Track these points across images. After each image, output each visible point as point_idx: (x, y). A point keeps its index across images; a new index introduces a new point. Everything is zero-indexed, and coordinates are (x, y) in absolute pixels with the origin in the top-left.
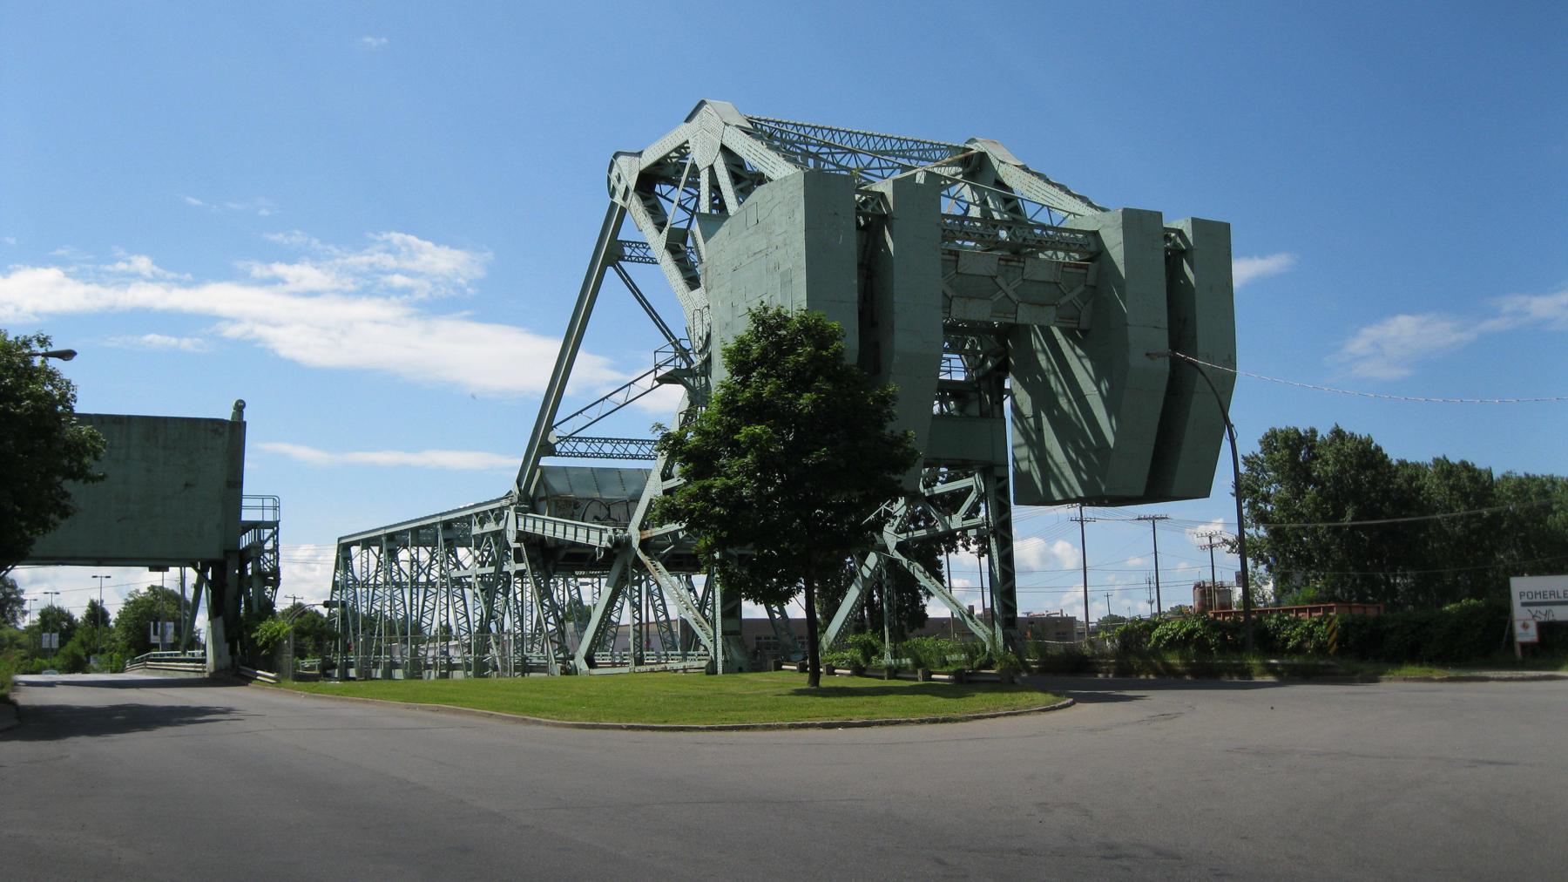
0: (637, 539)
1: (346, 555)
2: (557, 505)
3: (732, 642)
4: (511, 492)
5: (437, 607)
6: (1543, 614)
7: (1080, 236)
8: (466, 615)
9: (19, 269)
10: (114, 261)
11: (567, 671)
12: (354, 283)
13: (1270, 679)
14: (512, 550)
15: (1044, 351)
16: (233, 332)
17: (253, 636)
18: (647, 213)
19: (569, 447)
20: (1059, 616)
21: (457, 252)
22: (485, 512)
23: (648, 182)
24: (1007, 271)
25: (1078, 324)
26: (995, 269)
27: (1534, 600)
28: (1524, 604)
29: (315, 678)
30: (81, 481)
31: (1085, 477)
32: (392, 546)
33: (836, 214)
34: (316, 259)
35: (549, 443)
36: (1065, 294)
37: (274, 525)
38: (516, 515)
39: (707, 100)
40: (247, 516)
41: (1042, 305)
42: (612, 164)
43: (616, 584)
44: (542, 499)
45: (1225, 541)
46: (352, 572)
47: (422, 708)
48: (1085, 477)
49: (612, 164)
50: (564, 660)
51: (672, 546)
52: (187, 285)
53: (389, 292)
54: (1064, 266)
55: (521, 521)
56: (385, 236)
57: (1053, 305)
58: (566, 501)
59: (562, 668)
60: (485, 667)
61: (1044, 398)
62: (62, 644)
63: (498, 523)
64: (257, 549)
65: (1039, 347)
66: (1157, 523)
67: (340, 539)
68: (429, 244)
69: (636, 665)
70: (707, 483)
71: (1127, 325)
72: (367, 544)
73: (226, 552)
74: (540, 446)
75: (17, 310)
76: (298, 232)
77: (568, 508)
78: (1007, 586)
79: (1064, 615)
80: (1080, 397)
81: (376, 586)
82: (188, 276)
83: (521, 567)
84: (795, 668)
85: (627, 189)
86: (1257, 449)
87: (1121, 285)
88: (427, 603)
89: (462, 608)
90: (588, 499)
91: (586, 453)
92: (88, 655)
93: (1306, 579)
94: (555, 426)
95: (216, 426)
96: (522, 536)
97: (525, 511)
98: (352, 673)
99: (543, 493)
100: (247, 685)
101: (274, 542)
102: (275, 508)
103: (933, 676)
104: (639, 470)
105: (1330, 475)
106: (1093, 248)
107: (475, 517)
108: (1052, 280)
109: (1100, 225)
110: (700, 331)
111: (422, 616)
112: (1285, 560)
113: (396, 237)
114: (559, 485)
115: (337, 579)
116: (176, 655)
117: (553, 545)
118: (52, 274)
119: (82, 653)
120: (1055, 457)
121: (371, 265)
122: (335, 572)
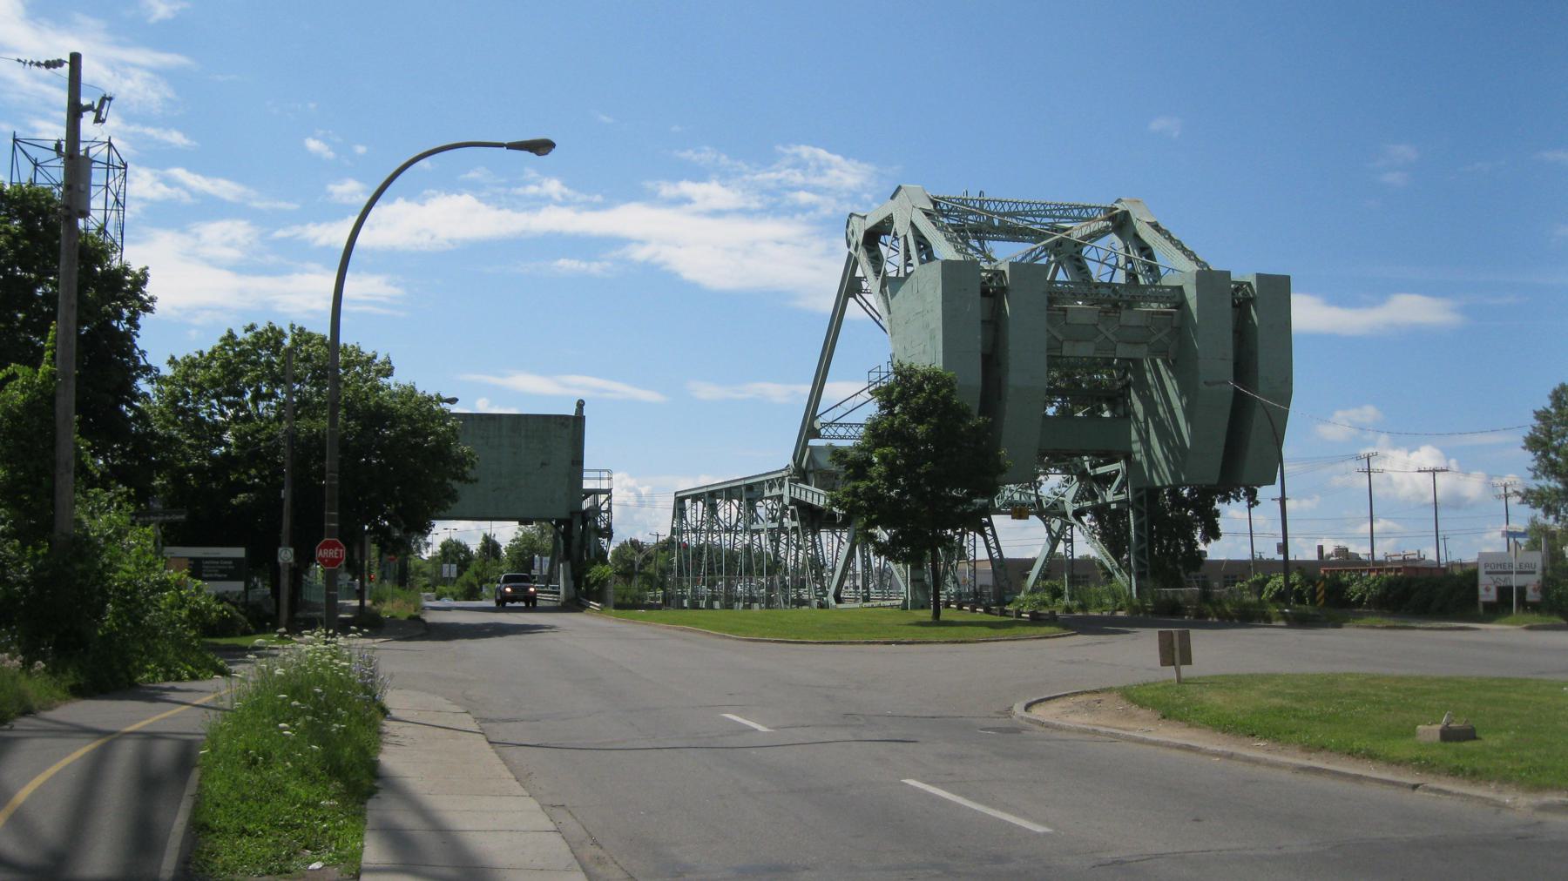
1: (681, 506)
2: (821, 477)
4: (788, 465)
6: (1502, 581)
7: (1168, 290)
9: (434, 196)
10: (524, 184)
11: (822, 606)
12: (759, 201)
13: (1282, 623)
15: (1150, 371)
16: (640, 254)
17: (587, 576)
20: (1416, 557)
21: (866, 166)
22: (772, 480)
27: (1496, 570)
28: (1487, 573)
29: (659, 607)
30: (463, 482)
34: (725, 177)
37: (608, 491)
39: (903, 186)
40: (587, 485)
41: (1136, 343)
44: (811, 472)
45: (1517, 493)
46: (686, 520)
47: (677, 629)
48: (1173, 468)
50: (820, 597)
52: (596, 207)
53: (795, 210)
56: (795, 150)
61: (1150, 408)
62: (460, 573)
66: (1438, 475)
68: (837, 158)
70: (857, 484)
73: (572, 513)
74: (808, 431)
75: (433, 237)
76: (707, 148)
82: (598, 198)
83: (795, 524)
86: (1547, 403)
89: (758, 541)
92: (481, 584)
94: (820, 415)
97: (797, 482)
99: (811, 468)
100: (582, 612)
103: (1023, 615)
106: (1177, 299)
113: (805, 151)
115: (675, 526)
116: (542, 587)
118: (466, 200)
119: (475, 581)
121: (779, 181)
122: (673, 520)
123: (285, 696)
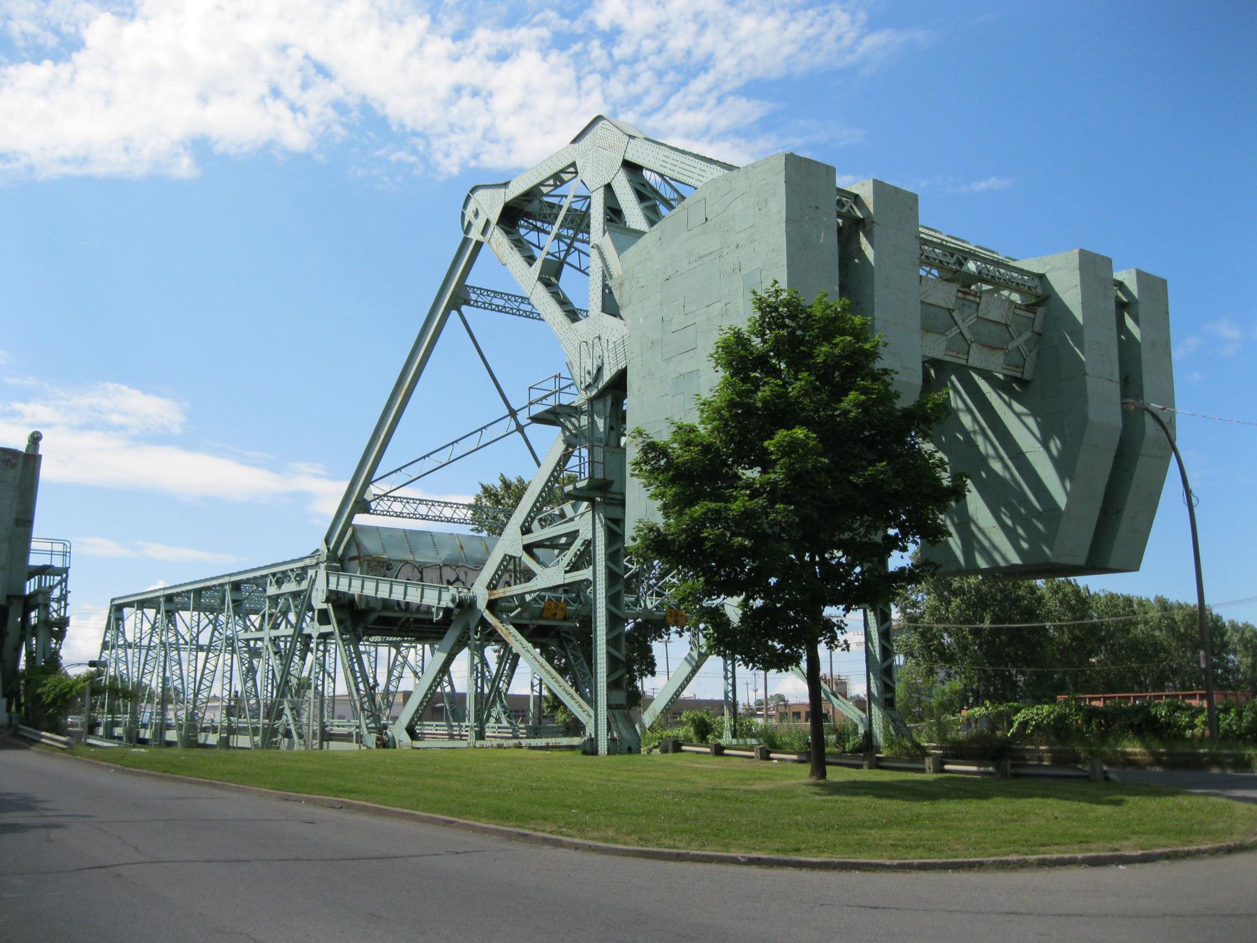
0: (484, 599)
1: (118, 615)
2: (369, 566)
3: (617, 716)
4: (318, 550)
5: (156, 671)
8: (182, 678)
14: (316, 612)
15: (969, 410)
18: (513, 247)
19: (384, 505)
23: (512, 216)
24: (964, 305)
25: (1023, 373)
26: (954, 301)
31: (1025, 545)
32: (171, 607)
33: (817, 208)
35: (365, 501)
36: (1013, 339)
38: (327, 573)
40: (35, 560)
41: (993, 348)
42: (468, 198)
43: (452, 649)
46: (123, 633)
48: (1025, 545)
49: (468, 198)
51: (519, 609)
54: (1015, 307)
55: (333, 579)
57: (1002, 349)
58: (379, 562)
59: (378, 739)
60: (275, 732)
63: (299, 583)
64: (40, 600)
65: (961, 405)
67: (113, 600)
69: (476, 739)
71: (1085, 374)
72: (142, 604)
73: (9, 597)
74: (356, 502)
77: (381, 567)
78: (887, 663)
79: (697, 698)
80: (1018, 456)
81: (149, 648)
83: (326, 629)
84: (708, 750)
85: (488, 223)
87: (1077, 331)
88: (147, 666)
89: (178, 672)
90: (401, 561)
91: (401, 513)
93: (949, 675)
95: (8, 457)
96: (334, 598)
97: (336, 569)
98: (118, 731)
100: (28, 748)
101: (62, 590)
102: (64, 554)
104: (451, 534)
105: (973, 586)
107: (271, 577)
108: (1003, 321)
109: (1048, 268)
110: (590, 366)
111: (142, 677)
112: (931, 657)
114: (371, 546)
117: (363, 606)
120: (981, 523)
122: (106, 632)
123: (961, 438)
